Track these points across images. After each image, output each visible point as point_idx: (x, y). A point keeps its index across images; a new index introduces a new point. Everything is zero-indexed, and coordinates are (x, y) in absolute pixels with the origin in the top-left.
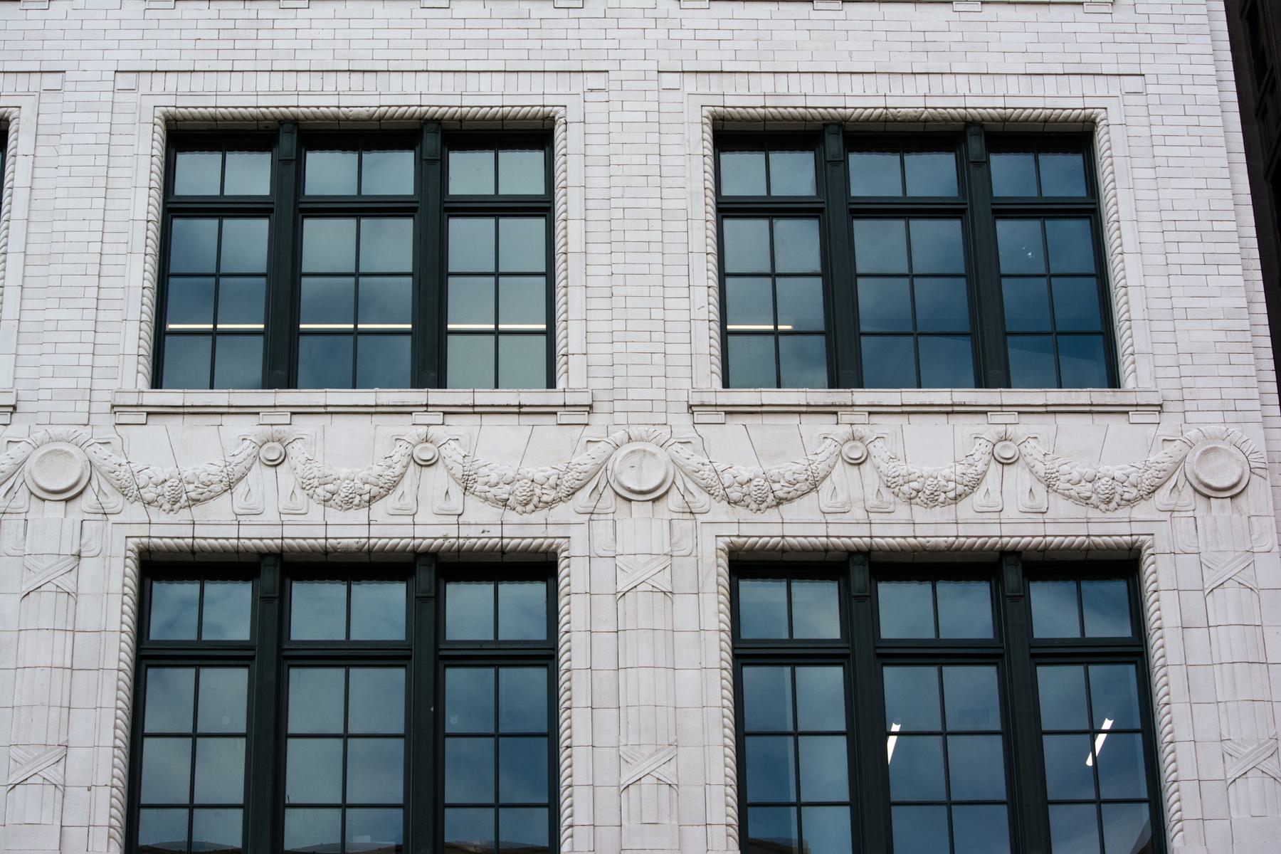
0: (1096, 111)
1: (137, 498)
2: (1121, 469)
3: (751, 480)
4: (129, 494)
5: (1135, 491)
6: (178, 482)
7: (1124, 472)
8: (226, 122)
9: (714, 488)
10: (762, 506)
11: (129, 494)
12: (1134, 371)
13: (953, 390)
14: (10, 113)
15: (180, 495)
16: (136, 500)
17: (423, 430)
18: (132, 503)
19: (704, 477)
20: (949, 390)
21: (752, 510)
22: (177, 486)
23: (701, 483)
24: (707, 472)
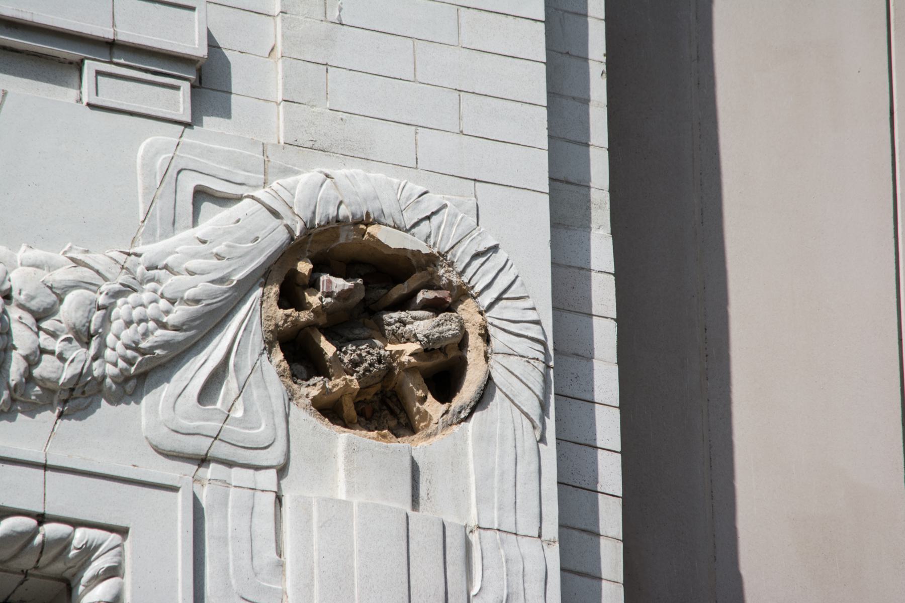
0: (81, 536)
14: (88, 552)
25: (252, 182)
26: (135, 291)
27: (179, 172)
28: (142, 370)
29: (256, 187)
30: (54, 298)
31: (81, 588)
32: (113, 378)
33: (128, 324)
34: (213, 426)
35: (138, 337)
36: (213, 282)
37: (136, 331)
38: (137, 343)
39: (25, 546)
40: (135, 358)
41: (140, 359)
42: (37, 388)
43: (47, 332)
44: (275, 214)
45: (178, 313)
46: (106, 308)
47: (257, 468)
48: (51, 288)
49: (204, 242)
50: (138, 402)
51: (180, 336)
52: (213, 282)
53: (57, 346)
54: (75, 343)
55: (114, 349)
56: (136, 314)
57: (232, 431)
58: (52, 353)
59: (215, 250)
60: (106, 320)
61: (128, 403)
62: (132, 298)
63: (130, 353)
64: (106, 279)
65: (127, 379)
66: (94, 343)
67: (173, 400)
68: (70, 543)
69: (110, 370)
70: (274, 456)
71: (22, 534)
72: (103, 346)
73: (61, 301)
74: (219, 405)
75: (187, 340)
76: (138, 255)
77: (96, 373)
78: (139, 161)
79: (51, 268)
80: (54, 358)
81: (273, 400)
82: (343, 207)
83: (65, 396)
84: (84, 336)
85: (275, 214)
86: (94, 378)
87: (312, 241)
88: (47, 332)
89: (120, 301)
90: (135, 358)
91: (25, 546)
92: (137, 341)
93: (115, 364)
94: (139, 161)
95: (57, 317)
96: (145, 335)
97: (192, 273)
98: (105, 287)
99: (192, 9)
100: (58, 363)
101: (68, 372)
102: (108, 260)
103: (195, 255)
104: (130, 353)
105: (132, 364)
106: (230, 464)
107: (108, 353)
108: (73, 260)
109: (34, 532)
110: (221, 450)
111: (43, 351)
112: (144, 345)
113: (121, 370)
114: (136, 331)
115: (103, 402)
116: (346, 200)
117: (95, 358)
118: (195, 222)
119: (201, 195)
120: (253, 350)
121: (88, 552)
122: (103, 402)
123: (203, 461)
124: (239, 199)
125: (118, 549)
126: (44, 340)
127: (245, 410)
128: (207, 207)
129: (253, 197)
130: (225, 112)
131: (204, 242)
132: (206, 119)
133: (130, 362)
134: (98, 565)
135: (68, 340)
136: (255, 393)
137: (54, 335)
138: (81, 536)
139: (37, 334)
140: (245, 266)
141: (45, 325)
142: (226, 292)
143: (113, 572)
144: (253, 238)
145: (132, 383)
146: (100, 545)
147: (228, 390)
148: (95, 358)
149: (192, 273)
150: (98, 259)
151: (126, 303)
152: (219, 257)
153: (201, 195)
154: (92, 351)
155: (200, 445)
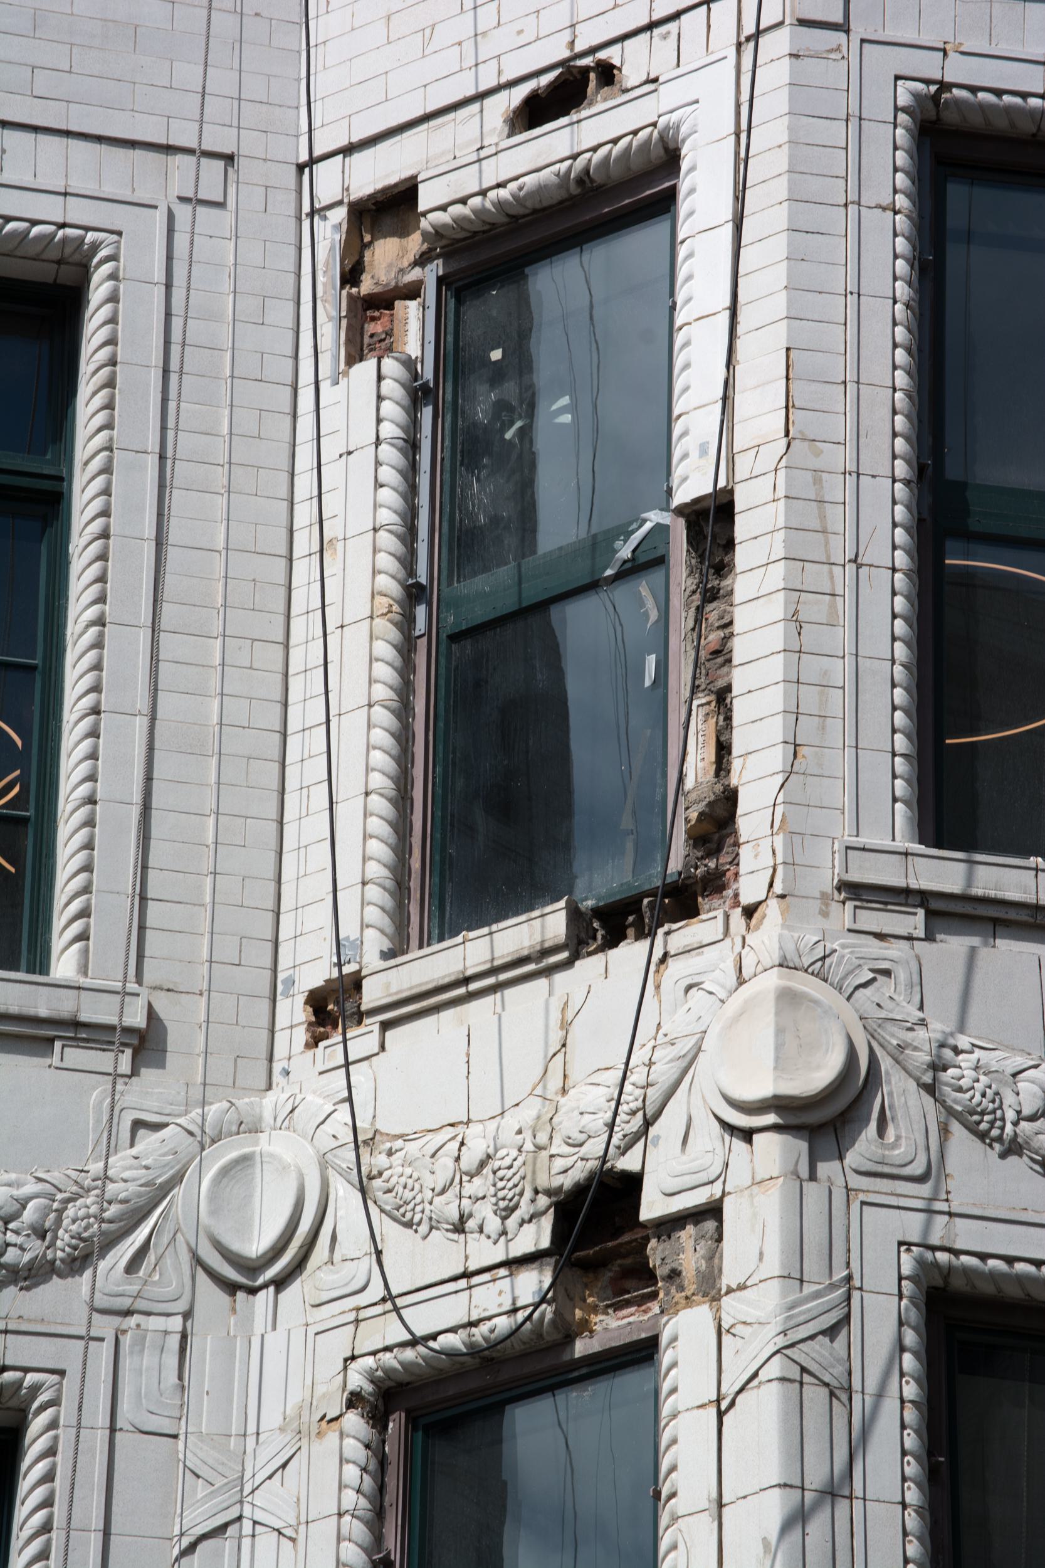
1: (434, 1224)
2: (9, 1185)
3: (489, 1157)
4: (417, 1219)
5: (36, 1248)
6: (514, 1153)
7: (16, 1192)
8: (498, 230)
9: (987, 1118)
10: (512, 1222)
11: (417, 1219)
12: (83, 936)
13: (494, 927)
14: (36, 1389)
15: (517, 1190)
16: (431, 1228)
17: (874, 948)
18: (425, 1238)
19: (964, 1083)
20: (485, 930)
21: (489, 1237)
22: (510, 1167)
23: (955, 1101)
24: (969, 1074)
25: (176, 1112)
26: (83, 1197)
27: (122, 1110)
28: (84, 1253)
29: (180, 1116)
30: (18, 1206)
31: (30, 1416)
32: (62, 1260)
33: (74, 1221)
34: (134, 1288)
35: (81, 1230)
36: (141, 1186)
37: (80, 1225)
38: (79, 1234)
39: (49, 243)
40: (78, 1245)
41: (82, 1245)
42: (4, 1271)
43: (12, 1231)
44: (191, 1133)
45: (112, 1211)
46: (60, 1212)
47: (168, 1315)
48: (16, 1200)
49: (136, 1158)
50: (81, 1276)
51: (113, 1226)
52: (141, 1186)
53: (19, 1240)
54: (33, 1237)
55: (63, 1240)
56: (81, 1213)
57: (152, 1291)
58: (15, 1245)
59: (144, 1163)
60: (59, 1221)
61: (73, 1277)
62: (79, 1203)
63: (74, 1241)
64: (60, 1191)
65: (74, 1260)
66: (49, 1236)
67: (106, 1272)
68: (22, 1384)
69: (60, 1254)
70: (182, 1306)
71: (50, 234)
72: (56, 1237)
73: (24, 1207)
74: (141, 1273)
75: (117, 1230)
76: (88, 1172)
77: (49, 1258)
78: (92, 1102)
79: (18, 1184)
80: (17, 1249)
81: (183, 1266)
82: (243, 1125)
83: (26, 1274)
84: (40, 1233)
85: (191, 1133)
86: (47, 1261)
87: (219, 580)
88: (12, 1231)
89: (70, 1205)
90: (78, 1245)
91: (49, 243)
92: (108, 445)
93: (63, 1250)
94: (92, 1102)
95: (20, 1220)
96: (86, 1229)
97: (125, 1181)
98: (59, 1196)
99: (156, 207)
100: (19, 1252)
101: (27, 1257)
102: (64, 1177)
103: (131, 1168)
104: (74, 1241)
105: (76, 1250)
106: (148, 1314)
107: (59, 1243)
108: (36, 1178)
109: (54, 234)
110: (141, 1305)
111: (8, 1245)
112: (85, 1235)
113: (69, 1255)
114: (80, 1225)
115: (55, 1276)
116: (245, 1121)
117: (48, 1248)
118: (132, 1145)
119: (138, 1124)
120: (169, 1232)
121: (36, 1389)
122: (55, 1276)
123: (128, 1313)
124: (166, 1125)
125: (57, 1386)
126: (10, 1237)
127: (160, 1274)
128: (142, 1132)
129: (177, 1124)
130: (161, 1064)
131: (136, 1158)
132: (143, 1071)
133: (75, 1248)
134: (43, 1398)
135: (28, 1235)
136: (168, 1261)
137: (17, 1232)
138: (31, 1378)
139: (5, 1234)
140: (165, 1173)
141: (11, 1226)
142: (150, 1192)
143: (54, 1402)
144: (173, 1152)
145: (78, 1263)
146: (44, 1384)
147: (149, 1262)
148: (48, 1248)
149: (125, 1181)
150: (55, 1176)
151: (75, 1206)
152: (147, 1168)
153: (138, 1124)
154: (46, 1243)
155: (125, 1303)
